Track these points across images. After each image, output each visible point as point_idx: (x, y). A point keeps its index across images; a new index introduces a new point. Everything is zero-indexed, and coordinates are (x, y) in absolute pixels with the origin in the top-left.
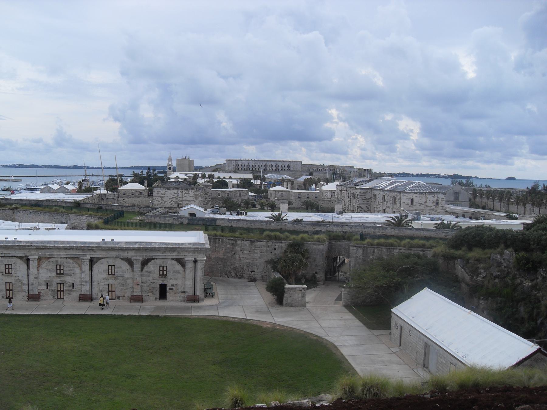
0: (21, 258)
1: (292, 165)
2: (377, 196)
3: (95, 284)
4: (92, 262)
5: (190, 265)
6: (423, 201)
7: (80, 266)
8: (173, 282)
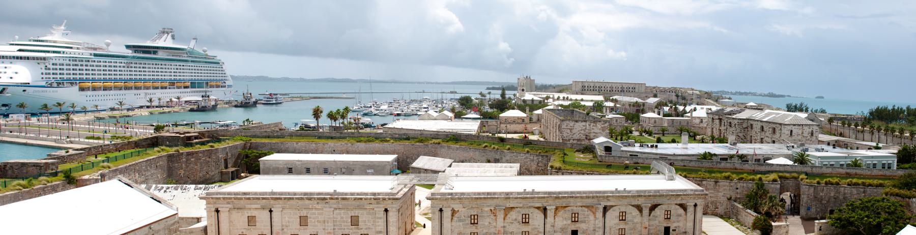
0: (538, 208)
1: (637, 87)
2: (754, 126)
3: (607, 229)
4: (605, 209)
5: (691, 209)
6: (800, 132)
7: (594, 213)
8: (675, 225)
